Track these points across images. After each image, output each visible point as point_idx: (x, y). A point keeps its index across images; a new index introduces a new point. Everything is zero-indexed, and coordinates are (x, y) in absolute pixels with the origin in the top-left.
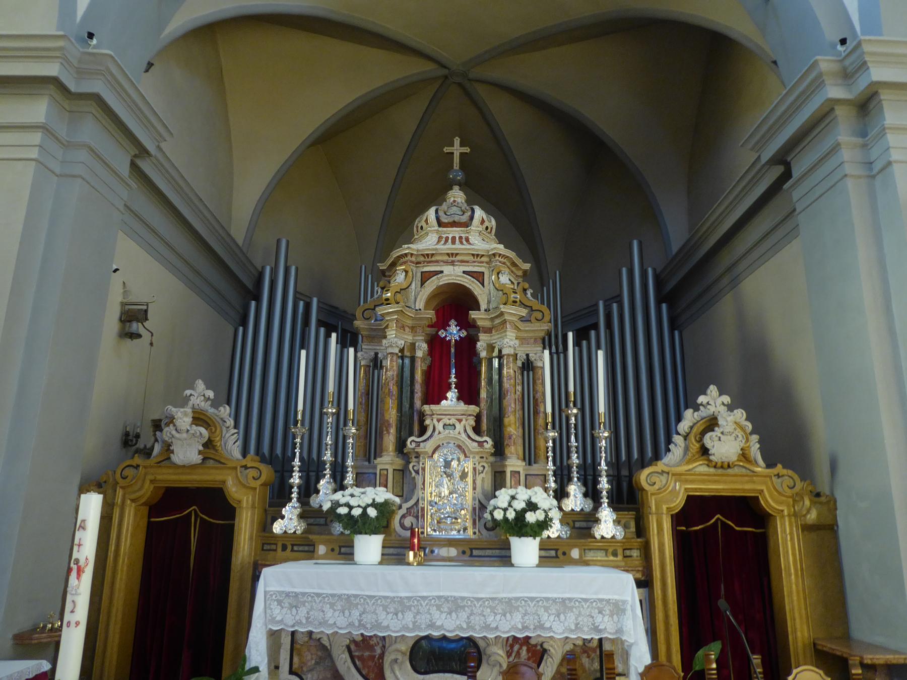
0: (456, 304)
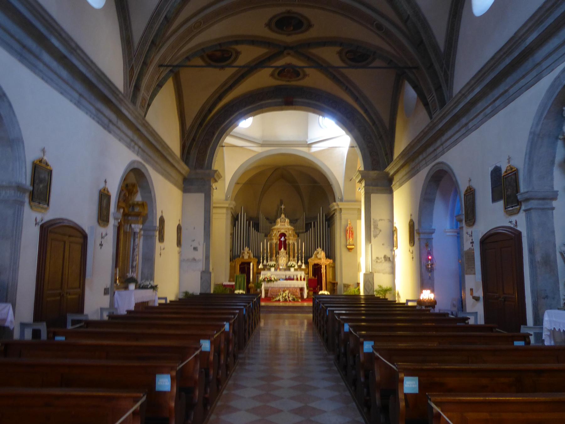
0: (283, 235)
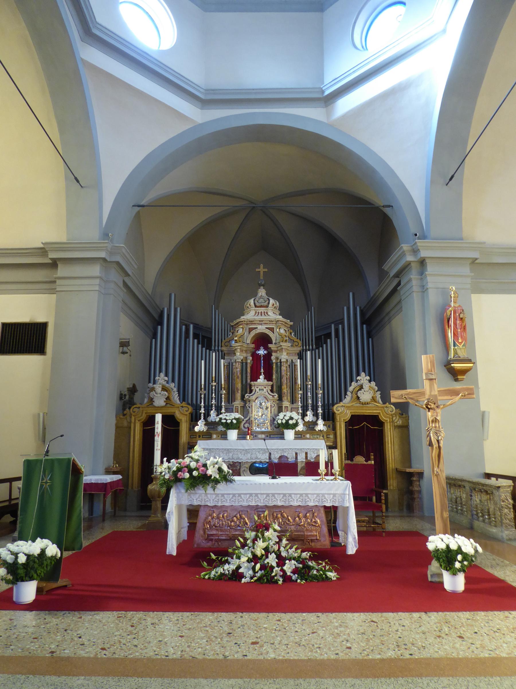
0: (263, 340)
